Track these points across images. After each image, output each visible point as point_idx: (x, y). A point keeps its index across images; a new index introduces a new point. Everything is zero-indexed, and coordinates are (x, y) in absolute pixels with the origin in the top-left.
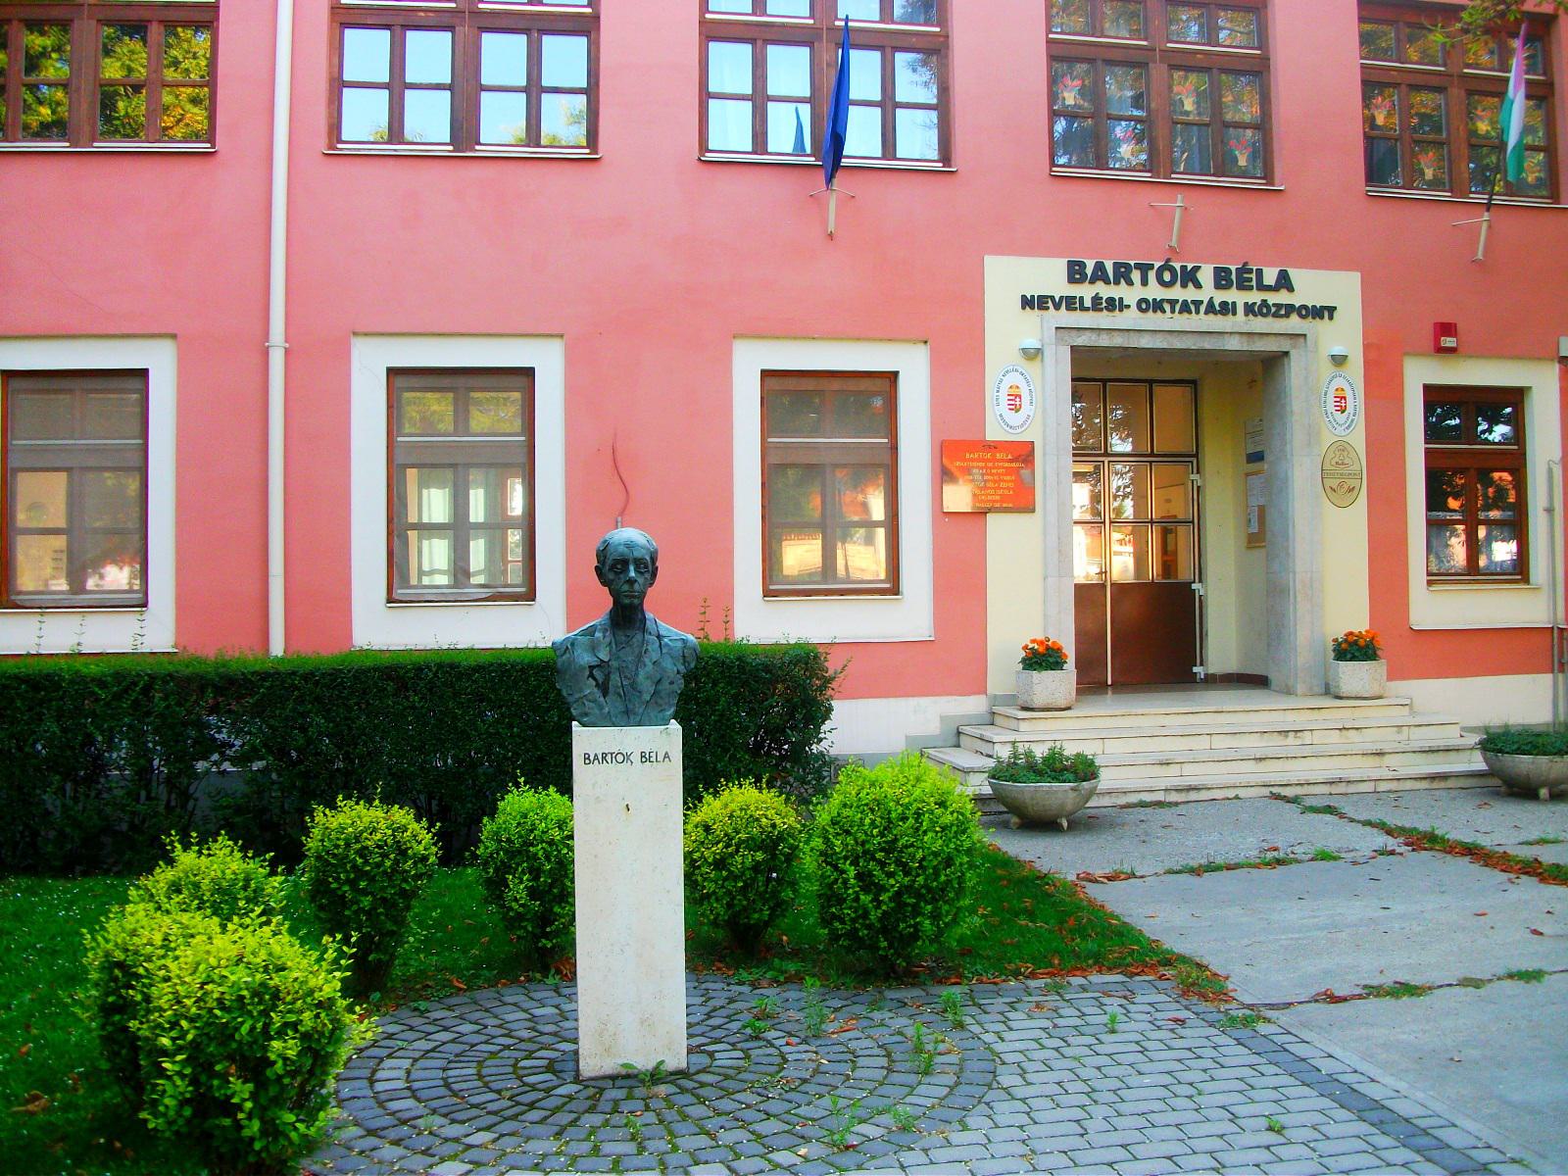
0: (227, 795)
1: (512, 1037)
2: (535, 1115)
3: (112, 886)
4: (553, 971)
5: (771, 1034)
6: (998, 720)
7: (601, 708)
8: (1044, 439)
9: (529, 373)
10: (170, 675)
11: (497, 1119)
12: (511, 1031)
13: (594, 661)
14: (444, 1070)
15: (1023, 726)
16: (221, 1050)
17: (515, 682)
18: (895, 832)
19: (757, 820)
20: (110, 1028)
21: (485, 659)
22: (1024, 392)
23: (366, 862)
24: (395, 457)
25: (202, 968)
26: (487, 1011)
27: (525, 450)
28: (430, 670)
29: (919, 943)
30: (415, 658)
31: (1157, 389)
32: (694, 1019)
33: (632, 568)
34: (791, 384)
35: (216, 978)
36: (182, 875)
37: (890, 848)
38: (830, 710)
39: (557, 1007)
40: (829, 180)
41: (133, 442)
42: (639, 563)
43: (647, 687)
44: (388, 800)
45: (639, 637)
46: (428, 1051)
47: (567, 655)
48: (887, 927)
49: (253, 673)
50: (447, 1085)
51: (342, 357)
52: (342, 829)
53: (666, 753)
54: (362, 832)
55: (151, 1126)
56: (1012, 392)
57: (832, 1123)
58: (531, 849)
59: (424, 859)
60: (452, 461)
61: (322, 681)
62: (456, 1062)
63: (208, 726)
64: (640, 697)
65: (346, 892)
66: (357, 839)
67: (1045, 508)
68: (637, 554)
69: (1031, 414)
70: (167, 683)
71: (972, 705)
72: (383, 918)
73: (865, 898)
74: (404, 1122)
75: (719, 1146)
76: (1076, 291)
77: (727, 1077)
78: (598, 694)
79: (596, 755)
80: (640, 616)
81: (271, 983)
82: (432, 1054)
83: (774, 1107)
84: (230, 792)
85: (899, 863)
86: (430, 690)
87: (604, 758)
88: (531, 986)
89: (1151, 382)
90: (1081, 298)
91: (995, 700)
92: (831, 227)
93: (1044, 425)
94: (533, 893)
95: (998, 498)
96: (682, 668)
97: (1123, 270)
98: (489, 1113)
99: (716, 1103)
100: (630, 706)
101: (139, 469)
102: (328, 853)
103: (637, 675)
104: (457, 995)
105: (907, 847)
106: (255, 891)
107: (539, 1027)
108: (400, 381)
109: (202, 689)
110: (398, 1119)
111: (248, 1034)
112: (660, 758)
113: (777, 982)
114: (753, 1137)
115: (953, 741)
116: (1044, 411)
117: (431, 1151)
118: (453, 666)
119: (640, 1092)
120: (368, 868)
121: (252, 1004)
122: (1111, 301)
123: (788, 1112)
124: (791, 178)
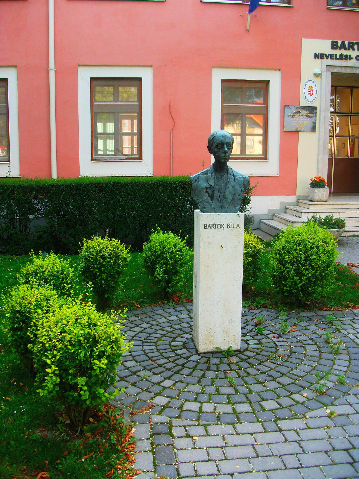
0: (41, 227)
1: (164, 330)
2: (186, 371)
3: (4, 259)
4: (171, 300)
5: (266, 332)
6: (300, 204)
7: (211, 205)
9: (140, 79)
10: (20, 186)
11: (172, 373)
12: (163, 327)
13: (208, 186)
14: (142, 346)
15: (311, 207)
16: (72, 364)
17: (141, 189)
18: (308, 253)
19: (249, 245)
20: (16, 337)
21: (129, 180)
23: (104, 261)
24: (93, 109)
25: (60, 324)
26: (150, 317)
27: (139, 107)
28: (111, 184)
29: (315, 295)
30: (105, 180)
31: (354, 90)
32: (245, 331)
33: (226, 146)
34: (231, 84)
35: (67, 330)
36: (37, 268)
37: (307, 259)
38: (249, 200)
39: (177, 316)
40: (251, 11)
41: (2, 104)
43: (229, 197)
44: (111, 236)
45: (226, 175)
46: (133, 337)
47: (196, 183)
48: (303, 289)
49: (49, 185)
50: (146, 354)
52: (94, 247)
53: (238, 224)
54: (102, 249)
55: (42, 394)
57: (309, 378)
58: (164, 255)
59: (125, 259)
60: (113, 111)
61: (73, 188)
62: (145, 342)
63: (34, 203)
64: (227, 201)
65: (97, 272)
66: (100, 252)
67: (319, 130)
68: (227, 141)
70: (19, 188)
71: (291, 199)
72: (110, 281)
73: (296, 278)
74: (134, 373)
75: (268, 390)
76: (334, 52)
77: (257, 354)
78: (209, 199)
79: (209, 225)
80: (226, 167)
81: (92, 333)
82: (135, 338)
83: (284, 370)
84: (41, 226)
85: (310, 265)
86: (111, 191)
87: (212, 226)
88: (165, 306)
89: (352, 87)
90: (336, 55)
91: (299, 197)
92: (248, 27)
93: (321, 101)
94: (165, 272)
96: (243, 189)
97: (351, 45)
98: (167, 369)
99: (258, 367)
100: (223, 205)
101: (6, 114)
102: (89, 257)
103: (225, 191)
104: (137, 310)
105: (313, 259)
106: (65, 275)
107: (174, 326)
108: (95, 83)
109: (31, 191)
110: (131, 372)
111: (84, 357)
112: (235, 227)
113: (258, 307)
114: (281, 386)
115: (284, 211)
116: (321, 96)
117: (149, 390)
118: (119, 183)
119: (225, 360)
120: (105, 263)
121: (84, 343)
122: (346, 56)
123: (289, 372)
124: (234, 9)
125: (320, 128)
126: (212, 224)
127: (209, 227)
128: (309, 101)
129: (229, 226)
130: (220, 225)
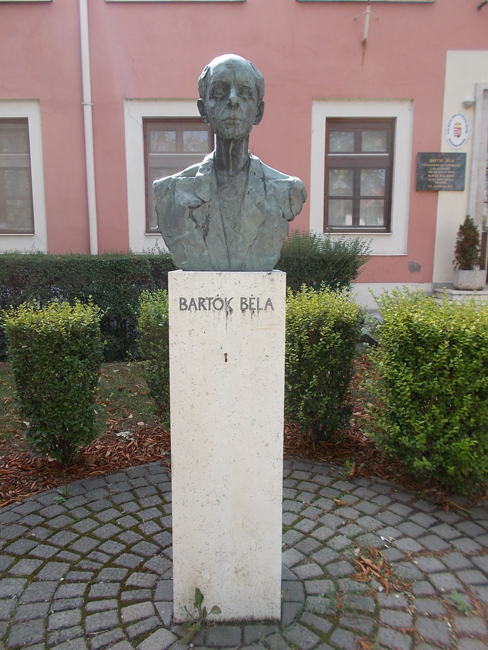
8: (472, 154)
22: (463, 127)
42: (242, 90)
51: (119, 113)
53: (269, 300)
56: (456, 126)
69: (466, 138)
78: (198, 234)
79: (193, 300)
87: (201, 304)
91: (437, 285)
92: (366, 35)
95: (445, 183)
108: (149, 126)
112: (262, 305)
125: (471, 160)
126: (200, 299)
127: (193, 307)
128: (455, 146)
129: (244, 303)
130: (222, 301)
